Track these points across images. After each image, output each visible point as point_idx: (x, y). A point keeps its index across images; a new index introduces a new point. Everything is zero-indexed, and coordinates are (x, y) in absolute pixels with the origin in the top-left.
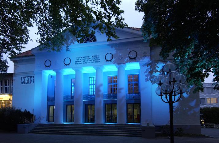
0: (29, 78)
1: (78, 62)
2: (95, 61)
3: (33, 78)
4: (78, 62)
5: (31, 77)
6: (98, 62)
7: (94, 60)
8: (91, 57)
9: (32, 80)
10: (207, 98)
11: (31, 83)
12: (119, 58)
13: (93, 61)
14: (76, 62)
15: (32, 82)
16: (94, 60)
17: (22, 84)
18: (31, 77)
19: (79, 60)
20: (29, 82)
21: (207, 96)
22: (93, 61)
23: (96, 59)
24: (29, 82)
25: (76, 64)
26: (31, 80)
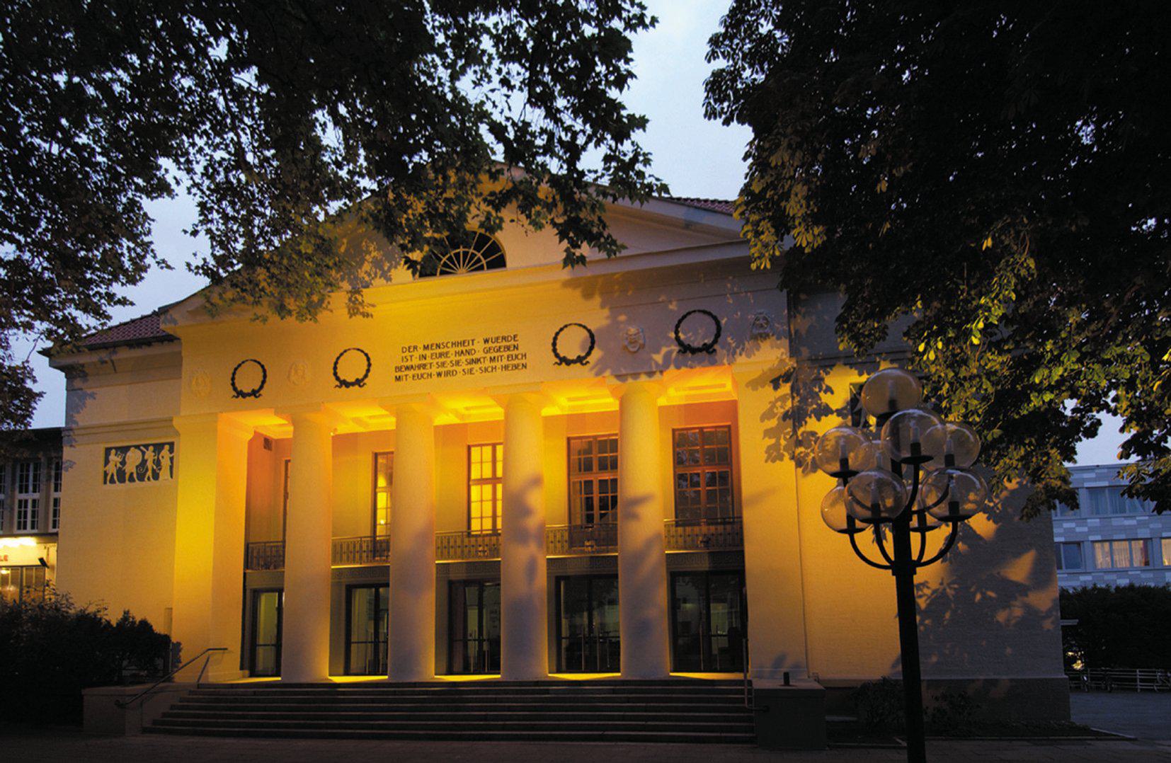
0: (150, 455)
1: (407, 368)
2: (498, 364)
3: (171, 451)
4: (407, 368)
5: (158, 448)
6: (516, 367)
7: (492, 360)
8: (479, 346)
9: (165, 463)
10: (1091, 538)
11: (156, 476)
12: (626, 347)
13: (487, 364)
14: (398, 369)
15: (164, 474)
16: (492, 360)
17: (112, 481)
18: (158, 448)
19: (416, 362)
20: (149, 473)
21: (1092, 531)
22: (487, 364)
23: (506, 354)
24: (149, 473)
25: (398, 379)
26: (158, 463)
